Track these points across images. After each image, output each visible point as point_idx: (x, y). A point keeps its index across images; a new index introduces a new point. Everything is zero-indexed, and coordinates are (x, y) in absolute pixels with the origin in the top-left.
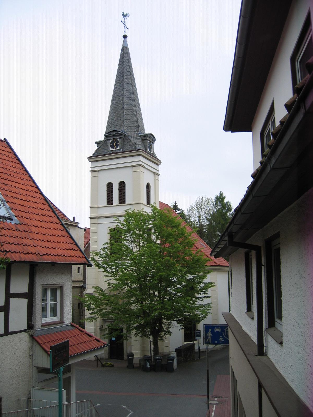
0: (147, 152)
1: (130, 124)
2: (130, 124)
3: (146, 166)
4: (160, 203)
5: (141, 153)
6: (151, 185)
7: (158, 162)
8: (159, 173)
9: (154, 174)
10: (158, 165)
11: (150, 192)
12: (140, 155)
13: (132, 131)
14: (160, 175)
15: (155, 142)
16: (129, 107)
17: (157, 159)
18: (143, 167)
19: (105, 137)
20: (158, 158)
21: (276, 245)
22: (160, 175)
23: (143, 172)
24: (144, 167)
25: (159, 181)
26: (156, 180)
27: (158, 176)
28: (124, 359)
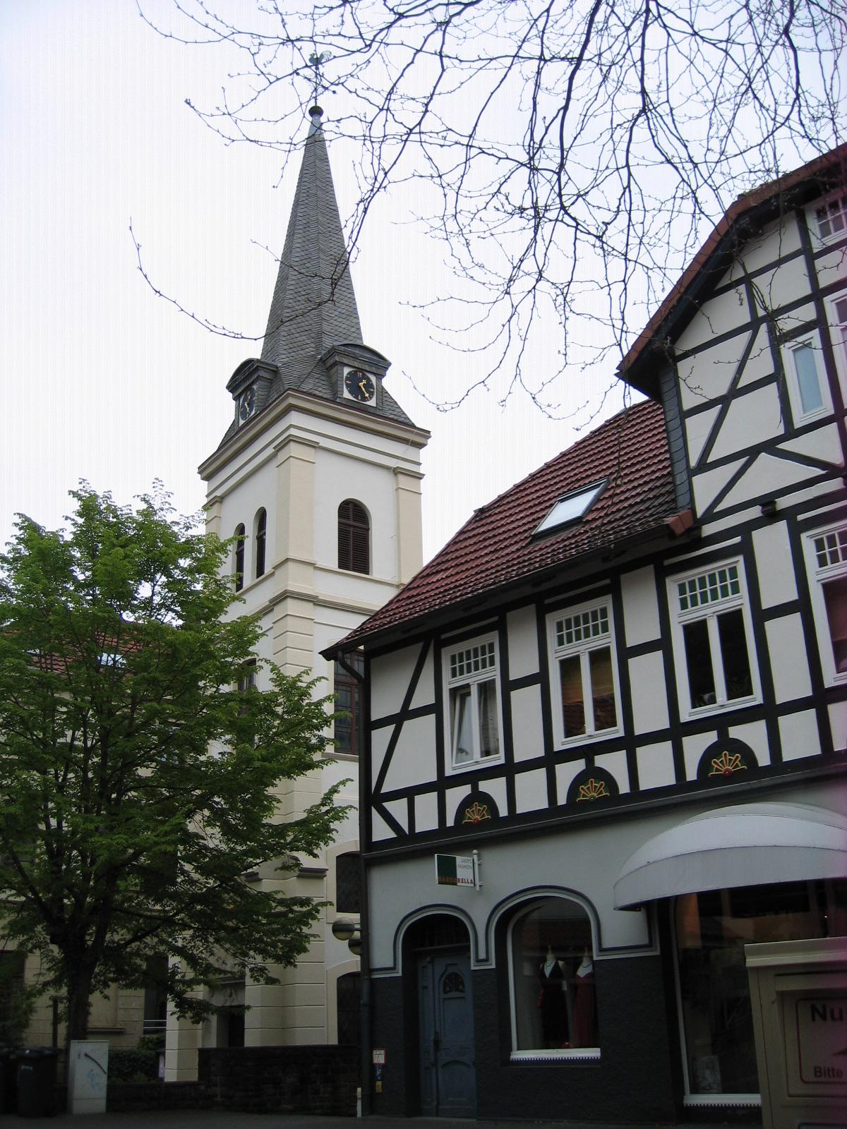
0: (338, 400)
1: (297, 335)
2: (297, 335)
3: (324, 442)
4: (138, 511)
5: (291, 401)
6: (367, 506)
7: (416, 437)
8: (421, 472)
9: (396, 474)
10: (421, 446)
11: (370, 532)
12: (291, 408)
13: (301, 352)
14: (424, 475)
15: (388, 372)
16: (300, 290)
17: (413, 426)
18: (314, 446)
19: (236, 398)
20: (417, 426)
21: (798, 1030)
22: (424, 475)
23: (314, 463)
24: (314, 447)
25: (422, 495)
26: (400, 490)
27: (415, 480)
28: (78, 1106)
